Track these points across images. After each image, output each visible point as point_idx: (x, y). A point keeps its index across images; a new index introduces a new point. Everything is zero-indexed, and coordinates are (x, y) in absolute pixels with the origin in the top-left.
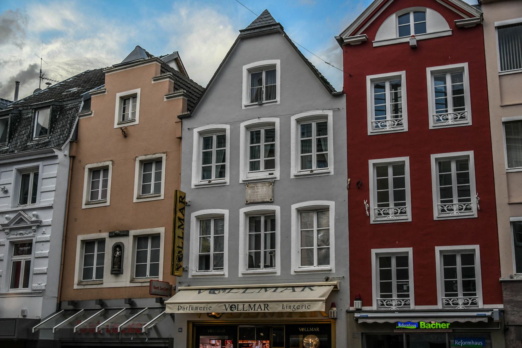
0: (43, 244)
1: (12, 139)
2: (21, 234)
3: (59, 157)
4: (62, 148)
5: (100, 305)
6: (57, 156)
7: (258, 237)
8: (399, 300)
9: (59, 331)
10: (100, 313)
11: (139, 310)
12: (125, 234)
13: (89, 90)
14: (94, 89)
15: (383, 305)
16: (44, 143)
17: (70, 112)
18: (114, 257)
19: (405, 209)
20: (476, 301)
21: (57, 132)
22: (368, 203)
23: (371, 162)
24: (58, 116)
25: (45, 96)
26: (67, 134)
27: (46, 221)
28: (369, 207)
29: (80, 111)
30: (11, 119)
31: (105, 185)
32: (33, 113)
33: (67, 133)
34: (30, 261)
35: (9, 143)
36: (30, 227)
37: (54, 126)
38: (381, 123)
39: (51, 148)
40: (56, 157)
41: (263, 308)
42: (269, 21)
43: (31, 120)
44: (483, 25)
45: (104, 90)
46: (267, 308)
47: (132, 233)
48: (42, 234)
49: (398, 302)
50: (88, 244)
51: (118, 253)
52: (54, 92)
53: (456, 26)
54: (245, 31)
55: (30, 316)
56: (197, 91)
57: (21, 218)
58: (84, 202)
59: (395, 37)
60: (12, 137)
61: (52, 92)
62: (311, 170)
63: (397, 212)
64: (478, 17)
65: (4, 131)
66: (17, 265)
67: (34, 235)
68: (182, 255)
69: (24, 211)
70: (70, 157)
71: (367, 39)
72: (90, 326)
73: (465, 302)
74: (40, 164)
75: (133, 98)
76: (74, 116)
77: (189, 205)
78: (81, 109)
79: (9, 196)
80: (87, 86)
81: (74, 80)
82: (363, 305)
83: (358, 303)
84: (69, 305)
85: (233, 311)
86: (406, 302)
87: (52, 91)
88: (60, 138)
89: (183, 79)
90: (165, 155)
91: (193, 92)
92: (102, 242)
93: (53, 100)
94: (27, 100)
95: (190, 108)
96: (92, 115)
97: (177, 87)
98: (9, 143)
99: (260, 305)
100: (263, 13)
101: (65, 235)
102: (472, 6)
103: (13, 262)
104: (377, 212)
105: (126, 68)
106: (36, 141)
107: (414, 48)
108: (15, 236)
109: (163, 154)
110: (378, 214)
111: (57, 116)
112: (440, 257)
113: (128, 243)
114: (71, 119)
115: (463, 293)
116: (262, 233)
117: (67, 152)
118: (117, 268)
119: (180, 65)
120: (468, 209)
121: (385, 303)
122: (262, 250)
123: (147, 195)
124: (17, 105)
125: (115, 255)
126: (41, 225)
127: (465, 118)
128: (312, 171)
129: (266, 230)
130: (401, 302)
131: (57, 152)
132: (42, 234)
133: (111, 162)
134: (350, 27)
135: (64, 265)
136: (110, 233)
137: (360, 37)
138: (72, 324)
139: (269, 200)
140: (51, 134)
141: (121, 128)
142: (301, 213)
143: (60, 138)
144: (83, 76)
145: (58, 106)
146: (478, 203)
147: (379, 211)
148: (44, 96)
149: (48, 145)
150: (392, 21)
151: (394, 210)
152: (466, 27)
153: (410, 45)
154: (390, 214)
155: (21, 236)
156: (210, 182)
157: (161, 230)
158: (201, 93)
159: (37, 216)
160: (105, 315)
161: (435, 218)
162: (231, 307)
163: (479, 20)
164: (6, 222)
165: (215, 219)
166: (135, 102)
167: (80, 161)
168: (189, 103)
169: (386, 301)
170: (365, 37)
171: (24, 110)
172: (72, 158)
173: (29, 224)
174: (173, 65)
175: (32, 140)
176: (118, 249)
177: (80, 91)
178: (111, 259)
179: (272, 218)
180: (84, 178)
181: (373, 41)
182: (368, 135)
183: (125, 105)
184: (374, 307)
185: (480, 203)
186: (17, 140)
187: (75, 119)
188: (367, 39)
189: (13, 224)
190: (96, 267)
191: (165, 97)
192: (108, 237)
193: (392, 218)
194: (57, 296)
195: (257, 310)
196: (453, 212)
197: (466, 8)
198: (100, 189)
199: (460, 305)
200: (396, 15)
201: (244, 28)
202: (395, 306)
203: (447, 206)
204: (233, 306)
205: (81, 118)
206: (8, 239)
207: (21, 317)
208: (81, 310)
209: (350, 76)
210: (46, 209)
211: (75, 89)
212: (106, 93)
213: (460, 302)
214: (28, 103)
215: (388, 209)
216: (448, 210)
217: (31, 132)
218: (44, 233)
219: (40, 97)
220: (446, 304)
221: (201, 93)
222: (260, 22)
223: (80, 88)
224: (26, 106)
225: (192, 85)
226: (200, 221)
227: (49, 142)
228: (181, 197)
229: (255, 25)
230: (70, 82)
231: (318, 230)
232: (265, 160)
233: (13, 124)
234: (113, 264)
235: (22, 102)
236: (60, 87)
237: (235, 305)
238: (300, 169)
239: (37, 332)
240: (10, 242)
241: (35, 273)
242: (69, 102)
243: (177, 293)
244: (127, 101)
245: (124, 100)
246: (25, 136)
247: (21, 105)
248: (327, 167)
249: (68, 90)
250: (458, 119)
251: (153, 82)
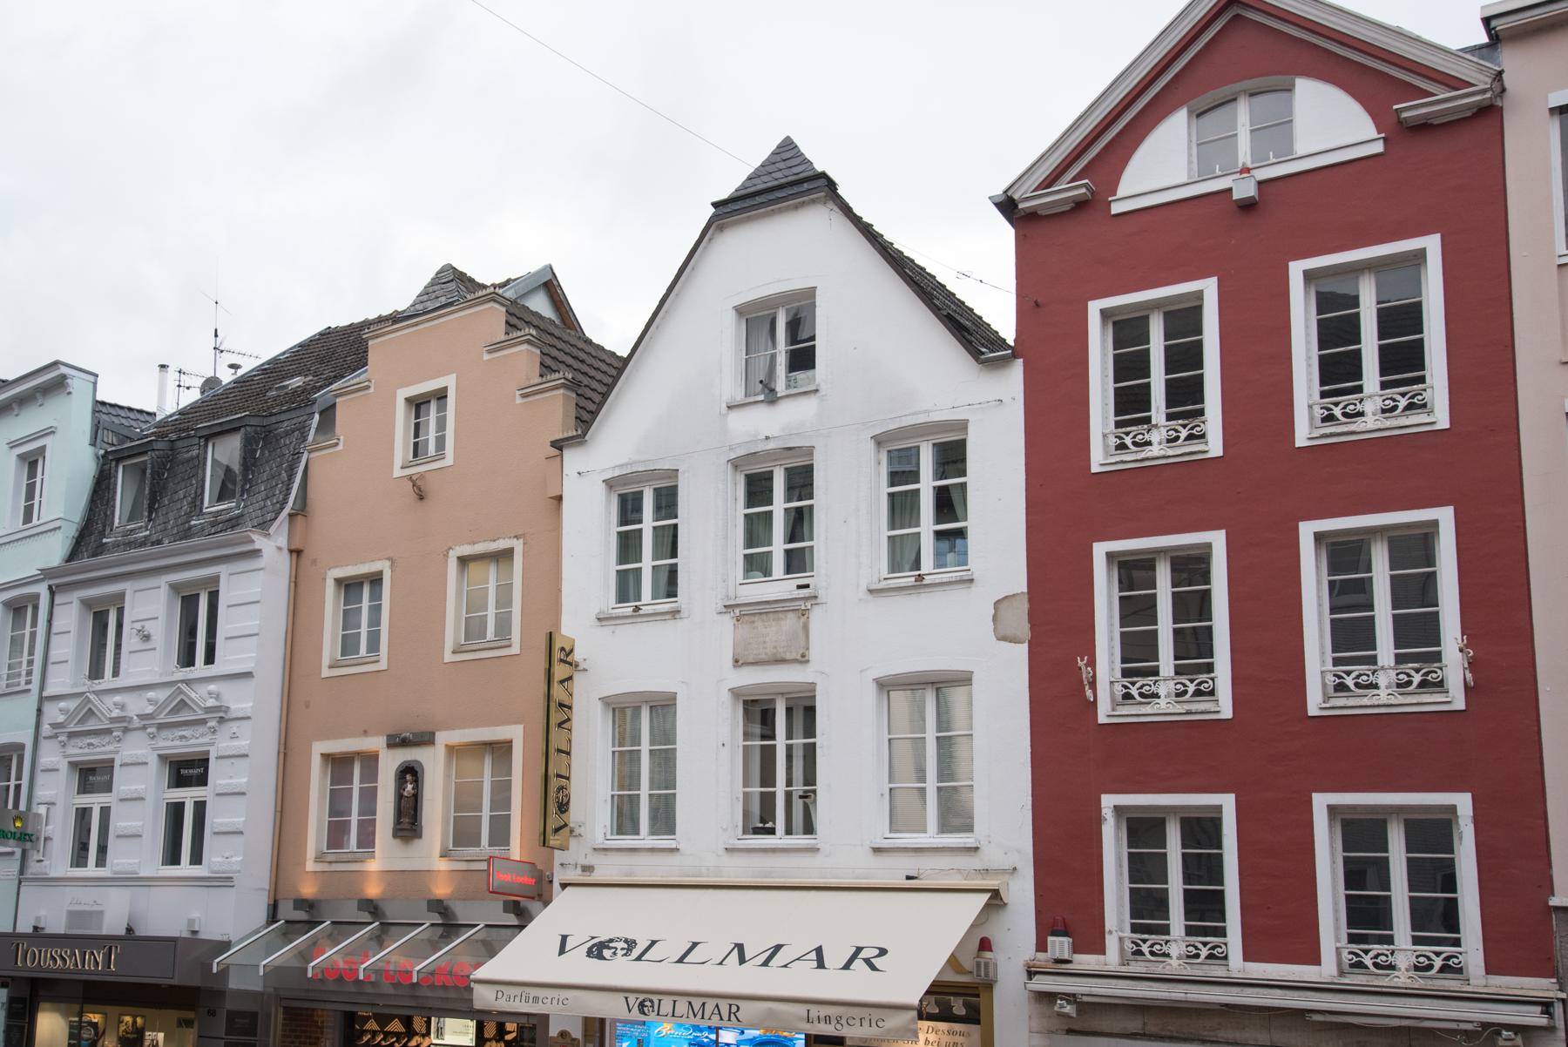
0: (233, 763)
1: (156, 510)
2: (182, 737)
3: (265, 552)
4: (271, 530)
5: (370, 912)
6: (259, 551)
7: (768, 755)
8: (1192, 943)
9: (275, 972)
10: (369, 933)
11: (463, 929)
12: (425, 739)
13: (331, 384)
14: (343, 380)
15: (1139, 953)
16: (230, 520)
17: (288, 442)
18: (400, 797)
19: (1211, 682)
20: (1460, 962)
21: (259, 493)
22: (1092, 663)
23: (1100, 550)
24: (259, 451)
25: (228, 402)
26: (281, 497)
27: (239, 708)
28: (1094, 676)
29: (311, 438)
30: (152, 464)
31: (375, 620)
32: (202, 448)
33: (280, 493)
34: (205, 801)
35: (149, 521)
36: (203, 722)
37: (251, 477)
38: (1135, 437)
39: (246, 533)
40: (256, 553)
41: (725, 1014)
42: (795, 170)
43: (196, 464)
44: (1502, 108)
45: (366, 384)
46: (734, 1013)
47: (443, 738)
48: (231, 738)
49: (1187, 946)
50: (339, 764)
51: (409, 787)
52: (248, 390)
53: (1400, 122)
54: (727, 204)
55: (211, 932)
56: (604, 367)
57: (182, 700)
58: (326, 661)
59: (1184, 180)
60: (157, 505)
61: (243, 391)
62: (917, 573)
63: (1185, 692)
64: (1482, 87)
65: (137, 491)
66: (175, 812)
67: (212, 741)
68: (568, 796)
69: (187, 682)
70: (291, 551)
71: (1093, 193)
72: (346, 962)
73: (1418, 962)
74: (223, 570)
75: (439, 399)
76: (296, 451)
77: (585, 670)
78: (312, 431)
79: (154, 649)
80: (327, 371)
81: (296, 356)
82: (1076, 949)
83: (1062, 943)
84: (295, 909)
85: (646, 1015)
86: (1213, 948)
87: (244, 389)
88: (265, 506)
89: (566, 338)
90: (521, 541)
91: (592, 372)
92: (370, 761)
93: (247, 413)
94: (187, 414)
95: (586, 416)
96: (340, 447)
97: (549, 362)
98: (149, 521)
99: (717, 1006)
100: (778, 147)
101: (283, 741)
102: (1460, 54)
103: (167, 803)
104: (1119, 691)
105: (417, 324)
106: (210, 516)
107: (1247, 206)
108: (169, 743)
109: (515, 539)
110: (1123, 695)
111: (256, 451)
112: (1331, 826)
113: (433, 761)
114: (290, 459)
115: (1413, 937)
116: (781, 742)
117: (282, 541)
118: (408, 823)
119: (558, 298)
120: (1433, 685)
121: (1145, 948)
122: (780, 789)
123: (476, 643)
124: (164, 427)
125: (402, 791)
126: (227, 717)
127: (1425, 406)
128: (920, 578)
129: (789, 736)
130: (1196, 948)
131: (259, 542)
132: (231, 738)
133: (387, 561)
134: (1039, 163)
135: (282, 812)
136: (389, 737)
137: (1069, 189)
138: (305, 955)
139: (799, 657)
140: (245, 496)
141: (410, 478)
142: (889, 691)
143: (265, 506)
144: (314, 343)
145: (258, 429)
146: (1466, 665)
147: (1125, 687)
148: (225, 403)
149: (238, 525)
150: (1177, 126)
151: (1176, 684)
152: (1435, 123)
153: (1234, 198)
154: (1163, 697)
155: (183, 743)
156: (637, 609)
157: (514, 733)
158: (614, 373)
159: (218, 697)
160: (379, 939)
161: (1313, 710)
162: (642, 1005)
163: (1488, 95)
164: (150, 709)
165: (652, 704)
166: (442, 408)
167: (314, 562)
168: (583, 403)
169: (1149, 943)
170: (1087, 189)
171: (179, 439)
172: (294, 555)
173: (201, 715)
174: (540, 305)
175: (201, 513)
176: (408, 777)
177: (309, 385)
178: (393, 800)
179: (808, 704)
180: (324, 603)
181: (1110, 199)
182: (1092, 471)
183: (418, 437)
184: (1111, 958)
185: (1473, 665)
186: (167, 514)
187: (298, 457)
188: (1093, 193)
189: (164, 713)
190: (359, 820)
191: (518, 393)
192: (385, 746)
193: (1168, 708)
194: (267, 887)
195: (710, 1019)
196: (1376, 692)
197: (1441, 61)
198: (364, 630)
199: (1400, 970)
200: (1190, 112)
201: (724, 195)
202: (1178, 958)
203: (1353, 675)
204: (648, 1003)
205: (313, 455)
206: (65, 756)
207: (186, 934)
208: (325, 922)
209: (1037, 304)
210: (243, 677)
211: (296, 382)
212: (372, 390)
213: (1404, 960)
214: (189, 422)
215: (1156, 681)
216: (1357, 685)
217: (199, 493)
218: (234, 737)
219: (215, 404)
220: (1352, 966)
221: (614, 373)
222: (774, 163)
223: (310, 378)
224: (183, 430)
225: (589, 354)
226: (614, 710)
227: (241, 516)
228: (563, 649)
229: (755, 185)
230: (285, 362)
231: (938, 738)
232: (934, 488)
233: (156, 476)
234: (399, 813)
235: (176, 420)
236: (262, 376)
237: (651, 1001)
238: (885, 573)
239: (224, 972)
240: (160, 756)
241: (217, 830)
242: (283, 417)
243: (557, 896)
244: (423, 407)
245: (418, 405)
246: (185, 503)
247: (173, 427)
248: (967, 565)
249: (281, 384)
250: (1396, 412)
251: (486, 357)
